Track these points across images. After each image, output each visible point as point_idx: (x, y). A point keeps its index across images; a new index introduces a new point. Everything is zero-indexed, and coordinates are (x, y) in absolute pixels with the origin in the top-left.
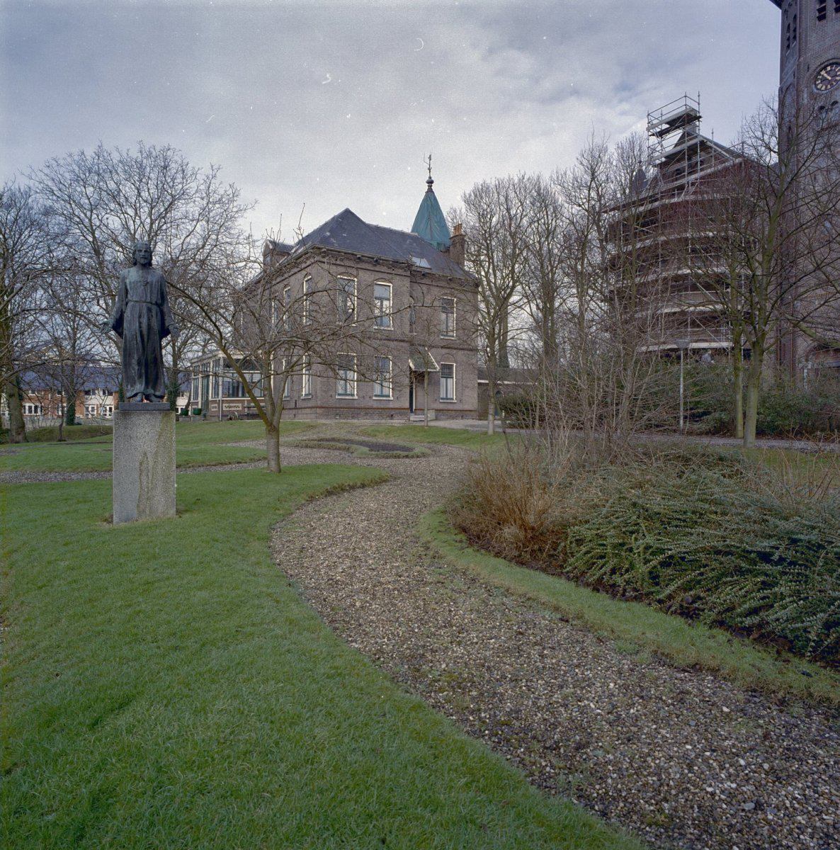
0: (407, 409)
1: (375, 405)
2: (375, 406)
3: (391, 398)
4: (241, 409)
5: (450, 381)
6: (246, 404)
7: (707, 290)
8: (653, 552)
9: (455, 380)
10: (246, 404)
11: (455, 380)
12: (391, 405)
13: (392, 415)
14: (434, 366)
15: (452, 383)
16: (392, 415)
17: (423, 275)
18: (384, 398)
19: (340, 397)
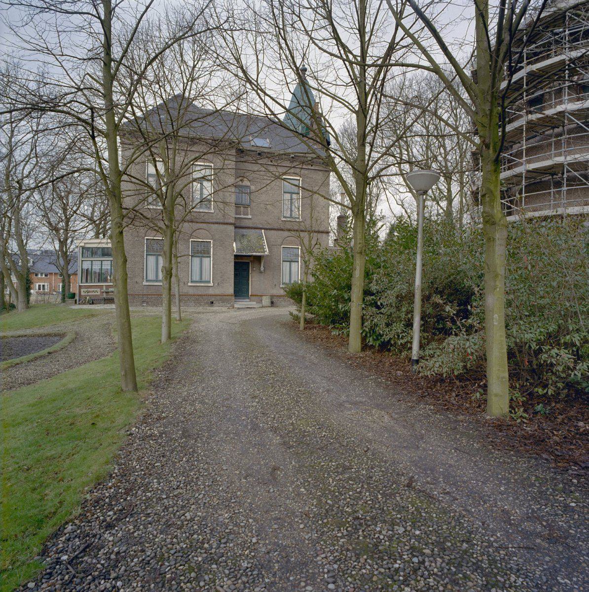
0: (231, 295)
1: (191, 291)
2: (190, 293)
3: (212, 284)
4: (99, 293)
5: (206, 261)
6: (104, 288)
7: (520, 112)
8: (518, 183)
9: (300, 264)
10: (104, 288)
11: (300, 264)
12: (211, 291)
13: (212, 303)
14: (264, 249)
15: (208, 263)
16: (212, 303)
17: (259, 154)
18: (202, 285)
19: (147, 284)
